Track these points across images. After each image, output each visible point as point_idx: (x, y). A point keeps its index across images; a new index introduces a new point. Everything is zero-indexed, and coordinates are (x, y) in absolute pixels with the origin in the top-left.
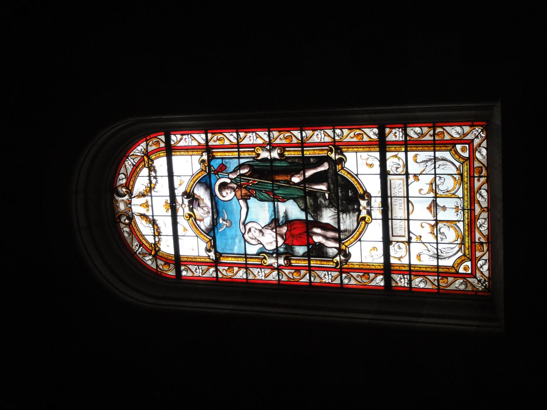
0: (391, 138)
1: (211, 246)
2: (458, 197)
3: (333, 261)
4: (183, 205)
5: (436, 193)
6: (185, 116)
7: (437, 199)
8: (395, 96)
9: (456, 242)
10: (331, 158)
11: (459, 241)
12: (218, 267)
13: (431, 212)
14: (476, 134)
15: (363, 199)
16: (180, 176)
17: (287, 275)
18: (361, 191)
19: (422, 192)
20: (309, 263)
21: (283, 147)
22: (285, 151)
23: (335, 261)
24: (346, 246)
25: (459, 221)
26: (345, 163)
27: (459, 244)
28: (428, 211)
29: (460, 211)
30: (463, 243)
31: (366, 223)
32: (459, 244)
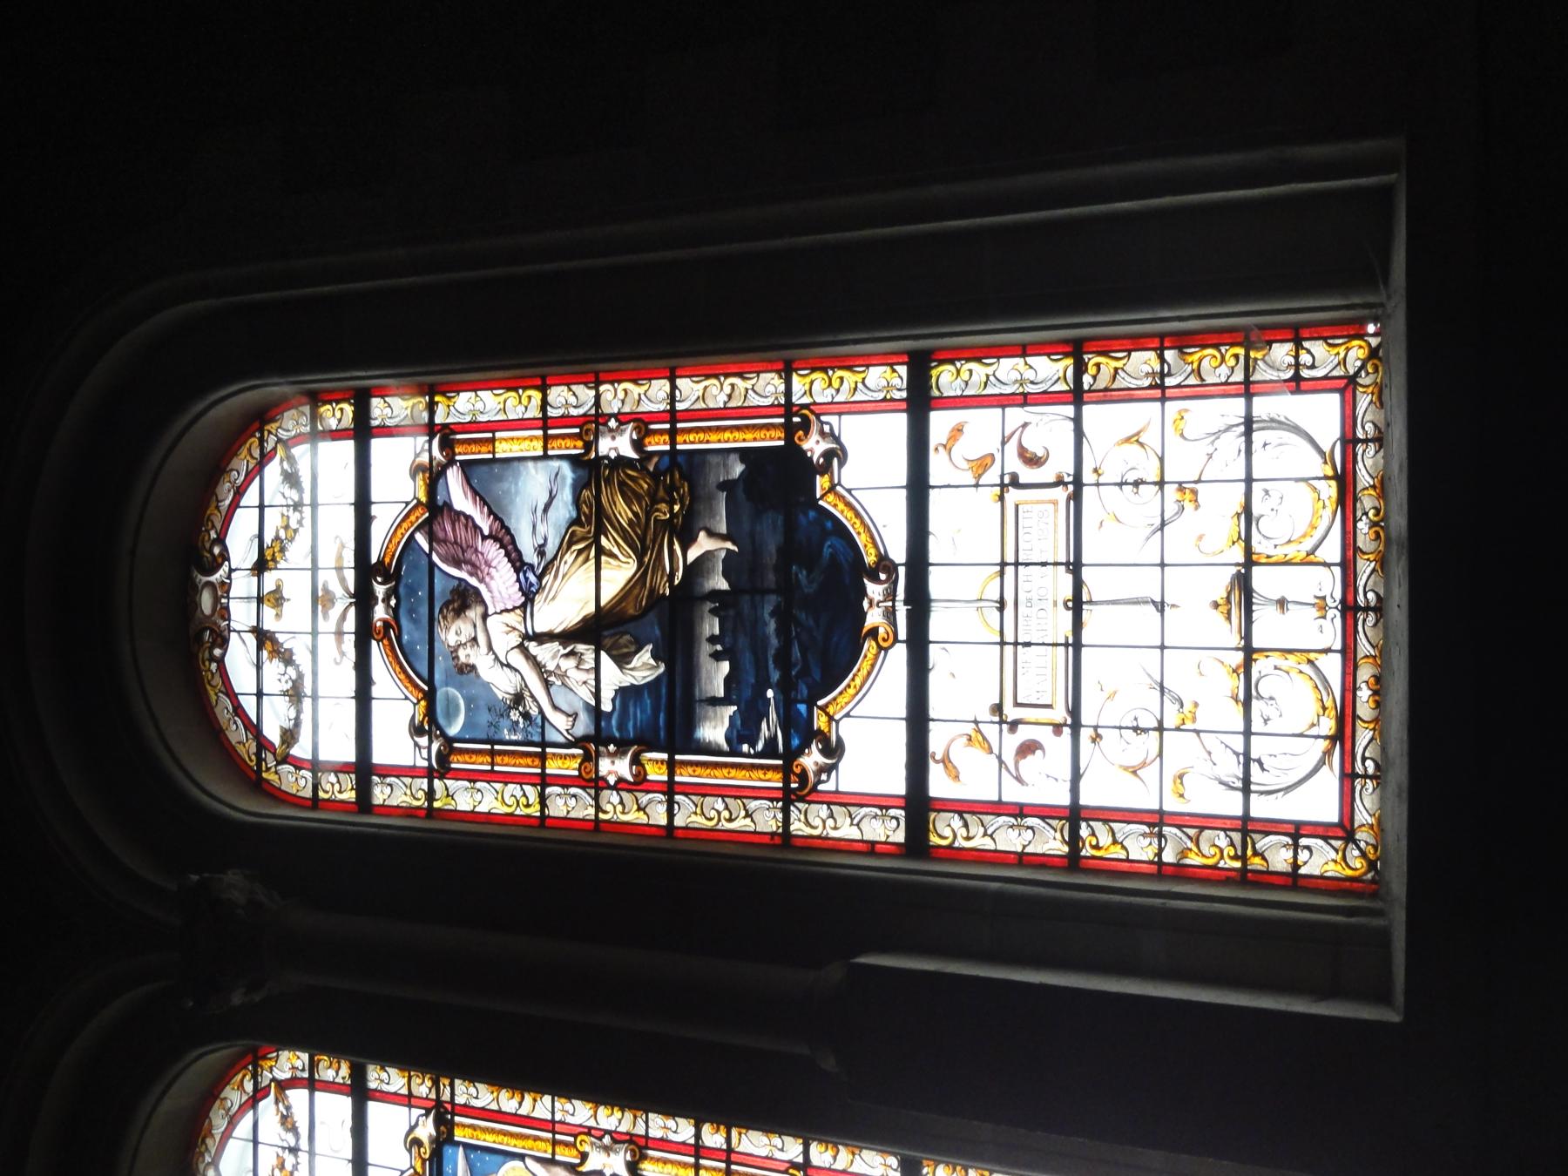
0: (349, 781)
2: (1325, 564)
3: (574, 1145)
5: (1248, 551)
6: (258, 296)
7: (1255, 569)
8: (1055, 227)
9: (1314, 731)
11: (1328, 726)
13: (1229, 618)
15: (876, 580)
16: (1160, 755)
18: (870, 559)
19: (1203, 544)
21: (640, 783)
22: (644, 1157)
25: (1327, 651)
26: (841, 465)
27: (1326, 737)
28: (1218, 617)
29: (1331, 613)
30: (1342, 735)
31: (880, 648)
32: (1326, 737)
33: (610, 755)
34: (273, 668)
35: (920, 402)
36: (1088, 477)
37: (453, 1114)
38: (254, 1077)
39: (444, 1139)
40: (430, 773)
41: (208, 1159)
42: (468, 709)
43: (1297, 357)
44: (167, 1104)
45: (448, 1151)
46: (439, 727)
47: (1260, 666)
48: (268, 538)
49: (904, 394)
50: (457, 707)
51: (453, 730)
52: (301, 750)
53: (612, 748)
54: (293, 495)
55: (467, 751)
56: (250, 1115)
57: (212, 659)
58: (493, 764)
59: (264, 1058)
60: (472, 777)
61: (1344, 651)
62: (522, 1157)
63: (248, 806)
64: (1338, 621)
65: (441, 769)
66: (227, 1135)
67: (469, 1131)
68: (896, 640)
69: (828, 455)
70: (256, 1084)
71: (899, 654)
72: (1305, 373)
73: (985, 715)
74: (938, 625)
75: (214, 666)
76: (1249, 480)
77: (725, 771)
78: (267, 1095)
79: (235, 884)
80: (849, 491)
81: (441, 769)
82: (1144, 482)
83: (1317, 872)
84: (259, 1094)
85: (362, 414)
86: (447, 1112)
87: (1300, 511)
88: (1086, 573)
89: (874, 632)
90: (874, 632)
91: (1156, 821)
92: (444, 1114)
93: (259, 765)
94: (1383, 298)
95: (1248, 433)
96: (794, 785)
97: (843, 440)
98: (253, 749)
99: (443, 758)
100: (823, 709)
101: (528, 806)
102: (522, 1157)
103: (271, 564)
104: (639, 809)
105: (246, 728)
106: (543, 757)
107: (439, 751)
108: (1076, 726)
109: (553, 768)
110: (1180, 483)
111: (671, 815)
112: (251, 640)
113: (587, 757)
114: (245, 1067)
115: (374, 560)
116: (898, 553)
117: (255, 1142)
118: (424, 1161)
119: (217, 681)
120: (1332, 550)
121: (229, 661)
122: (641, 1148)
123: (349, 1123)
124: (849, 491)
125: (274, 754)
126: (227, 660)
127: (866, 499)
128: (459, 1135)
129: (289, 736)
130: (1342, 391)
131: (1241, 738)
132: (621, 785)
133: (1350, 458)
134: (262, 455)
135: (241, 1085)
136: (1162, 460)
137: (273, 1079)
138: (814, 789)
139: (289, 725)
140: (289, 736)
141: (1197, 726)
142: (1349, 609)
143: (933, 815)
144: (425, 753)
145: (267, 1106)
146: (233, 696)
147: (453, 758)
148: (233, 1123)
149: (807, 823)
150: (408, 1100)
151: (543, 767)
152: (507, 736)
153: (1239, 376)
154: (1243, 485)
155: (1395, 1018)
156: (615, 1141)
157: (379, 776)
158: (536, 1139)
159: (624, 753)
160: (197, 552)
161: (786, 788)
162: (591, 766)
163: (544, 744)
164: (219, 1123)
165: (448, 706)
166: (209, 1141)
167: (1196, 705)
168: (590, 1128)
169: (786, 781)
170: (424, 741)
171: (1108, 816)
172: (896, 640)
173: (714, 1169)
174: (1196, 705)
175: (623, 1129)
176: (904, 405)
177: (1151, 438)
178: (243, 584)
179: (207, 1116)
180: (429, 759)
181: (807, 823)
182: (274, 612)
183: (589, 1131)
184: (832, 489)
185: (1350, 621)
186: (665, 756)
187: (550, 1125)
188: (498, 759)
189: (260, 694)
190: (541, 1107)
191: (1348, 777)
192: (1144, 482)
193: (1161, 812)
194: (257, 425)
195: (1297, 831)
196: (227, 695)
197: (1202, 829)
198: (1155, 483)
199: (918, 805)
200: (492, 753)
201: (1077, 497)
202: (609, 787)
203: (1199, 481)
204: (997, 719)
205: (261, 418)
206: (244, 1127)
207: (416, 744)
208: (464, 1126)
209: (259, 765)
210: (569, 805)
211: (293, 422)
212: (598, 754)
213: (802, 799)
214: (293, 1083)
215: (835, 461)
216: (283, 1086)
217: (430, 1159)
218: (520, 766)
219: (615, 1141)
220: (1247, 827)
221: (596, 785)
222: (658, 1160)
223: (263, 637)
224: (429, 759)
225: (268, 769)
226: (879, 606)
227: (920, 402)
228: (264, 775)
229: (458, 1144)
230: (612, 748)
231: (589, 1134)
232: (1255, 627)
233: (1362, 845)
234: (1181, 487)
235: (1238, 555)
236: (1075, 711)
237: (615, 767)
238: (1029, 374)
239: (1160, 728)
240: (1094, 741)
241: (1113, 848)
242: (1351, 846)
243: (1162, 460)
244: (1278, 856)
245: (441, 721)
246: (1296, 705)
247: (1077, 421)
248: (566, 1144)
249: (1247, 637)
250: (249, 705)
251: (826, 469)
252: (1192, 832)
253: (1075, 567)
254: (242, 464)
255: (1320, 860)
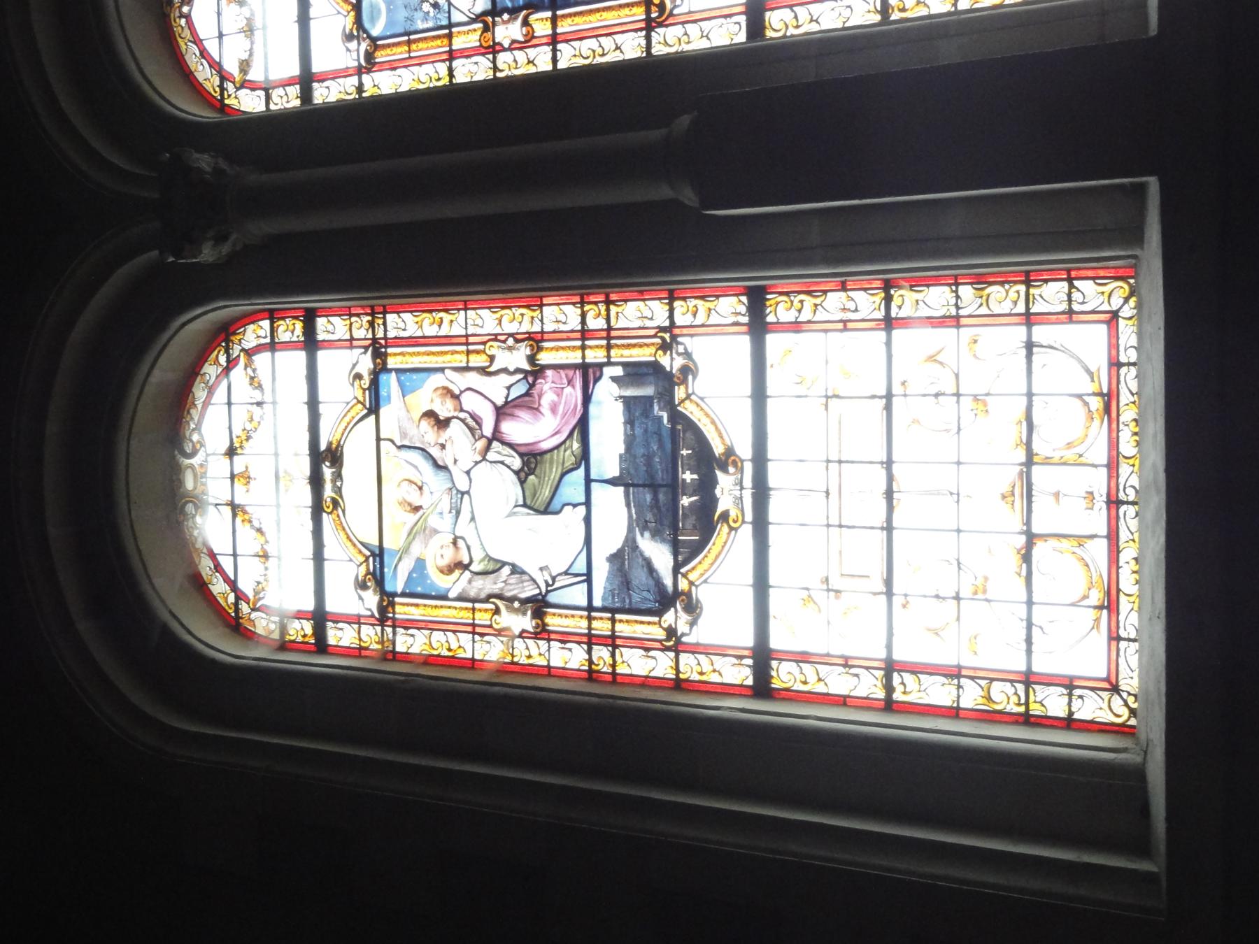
1: (368, 573)
3: (484, 352)
4: (344, 490)
5: (1030, 454)
10: (663, 368)
11: (1096, 597)
12: (892, 292)
14: (1115, 294)
15: (725, 471)
16: (958, 619)
17: (533, 653)
18: (718, 449)
20: (590, 624)
21: (529, 41)
22: (540, 349)
23: (665, 626)
24: (691, 583)
28: (1005, 507)
31: (731, 529)
33: (504, 22)
34: (243, 530)
35: (758, 326)
36: (897, 389)
37: (386, 347)
38: (227, 351)
39: (380, 369)
40: (360, 71)
41: (192, 426)
42: (389, 10)
43: (1069, 295)
44: (157, 376)
45: (383, 378)
46: (365, 31)
47: (1039, 550)
48: (237, 431)
49: (745, 320)
50: (379, 10)
51: (375, 32)
52: (255, 75)
53: (506, 16)
54: (257, 396)
55: (389, 46)
56: (224, 383)
57: (182, 16)
58: (409, 51)
59: (234, 334)
60: (392, 66)
61: (1109, 537)
62: (442, 370)
63: (226, 648)
64: (1104, 511)
65: (370, 64)
66: (206, 404)
67: (399, 358)
68: (743, 522)
69: (685, 370)
70: (228, 357)
71: (746, 532)
72: (1076, 307)
73: (815, 584)
74: (775, 510)
75: (183, 21)
76: (1030, 395)
77: (598, 15)
78: (236, 364)
79: (204, 161)
80: (702, 399)
81: (370, 64)
82: (943, 394)
83: (1089, 718)
84: (231, 363)
85: (310, 330)
86: (382, 346)
87: (1069, 426)
88: (896, 469)
89: (725, 516)
90: (725, 516)
91: (954, 674)
92: (378, 349)
93: (222, 94)
94: (1138, 252)
95: (1029, 355)
96: (654, 15)
97: (694, 357)
98: (217, 82)
99: (369, 56)
100: (684, 576)
101: (439, 79)
102: (442, 370)
103: (239, 451)
104: (529, 62)
105: (211, 66)
106: (450, 36)
107: (367, 52)
108: (889, 593)
109: (458, 43)
110: (975, 396)
111: (555, 60)
112: (227, 511)
113: (486, 29)
114: (219, 345)
115: (323, 447)
116: (745, 450)
117: (229, 404)
118: (364, 390)
119: (187, 33)
120: (1100, 454)
121: (195, 17)
122: (538, 342)
123: (304, 372)
124: (702, 399)
125: (234, 83)
126: (193, 15)
127: (715, 405)
128: (392, 362)
129: (245, 66)
130: (1108, 322)
131: (1024, 607)
132: (515, 46)
133: (1114, 379)
134: (228, 361)
135: (216, 361)
136: (957, 376)
137: (243, 350)
138: (671, 15)
139: (245, 56)
140: (245, 66)
141: (988, 596)
142: (1114, 503)
143: (768, 14)
144: (355, 55)
145: (238, 373)
146: (197, 41)
147: (378, 54)
148: (211, 391)
149: (666, 44)
150: (351, 342)
151: (450, 45)
152: (421, 25)
153: (1021, 308)
154: (1025, 399)
155: (1153, 183)
156: (517, 341)
157: (334, 622)
158: (453, 353)
159: (516, 19)
160: (178, 403)
161: (648, 20)
162: (489, 35)
163: (450, 26)
164: (200, 393)
165: (372, 12)
166: (193, 411)
167: (986, 579)
168: (496, 335)
169: (648, 12)
170: (353, 45)
171: (916, 669)
172: (743, 522)
173: (597, 347)
174: (986, 579)
175: (523, 330)
176: (744, 329)
177: (948, 357)
178: (218, 468)
179: (190, 391)
180: (358, 60)
181: (666, 44)
182: (245, 488)
183: (495, 338)
184: (688, 397)
185: (1113, 512)
186: (549, 14)
187: (466, 340)
188: (414, 47)
189: (235, 555)
190: (455, 322)
191: (1114, 638)
192: (943, 394)
193: (960, 668)
194: (223, 336)
195: (1069, 685)
196: (194, 42)
197: (992, 680)
198: (953, 395)
199: (762, 657)
200: (409, 42)
201: (888, 408)
202: (504, 50)
203: (988, 394)
204: (825, 587)
205: (225, 333)
206: (220, 394)
207: (348, 50)
208: (395, 354)
209: (222, 94)
210: (472, 71)
211: (254, 334)
212: (494, 24)
213: (661, 25)
214: (259, 349)
215: (690, 377)
216: (249, 353)
217: (369, 389)
218: (433, 48)
219: (517, 341)
220: (1029, 679)
221: (494, 49)
222: (552, 349)
223: (235, 508)
224: (358, 60)
225: (229, 96)
226: (730, 492)
227: (758, 326)
228: (227, 102)
229: (390, 371)
230: (506, 16)
231: (496, 340)
232: (1034, 515)
233: (1125, 695)
234: (976, 398)
235: (1021, 456)
236: (888, 582)
237: (508, 31)
238: (851, 306)
239: (957, 598)
240: (904, 606)
241: (917, 9)
242: (1116, 697)
243: (957, 376)
244: (1053, 703)
245: (367, 25)
246: (1068, 576)
247: (888, 344)
248: (478, 352)
249: (1028, 523)
250: (212, 47)
251: (684, 381)
252: (983, 683)
253: (888, 464)
254: (211, 370)
255: (1091, 708)
